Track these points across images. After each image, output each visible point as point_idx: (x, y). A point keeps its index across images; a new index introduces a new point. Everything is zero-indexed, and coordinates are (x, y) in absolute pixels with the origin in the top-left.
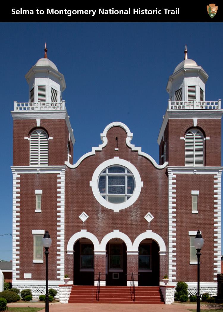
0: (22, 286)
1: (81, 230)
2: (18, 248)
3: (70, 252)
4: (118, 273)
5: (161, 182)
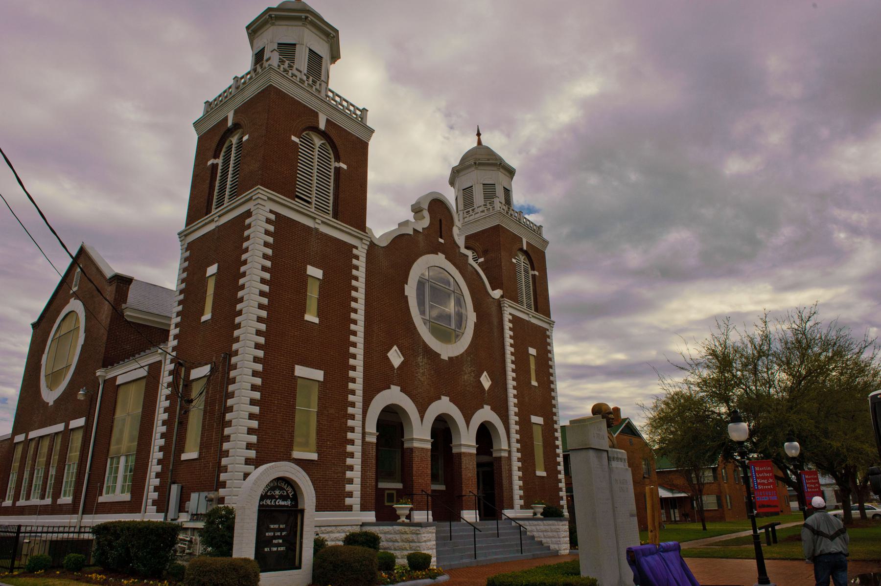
0: (329, 529)
1: (392, 386)
2: (256, 410)
3: (371, 434)
4: (394, 492)
5: (495, 321)
